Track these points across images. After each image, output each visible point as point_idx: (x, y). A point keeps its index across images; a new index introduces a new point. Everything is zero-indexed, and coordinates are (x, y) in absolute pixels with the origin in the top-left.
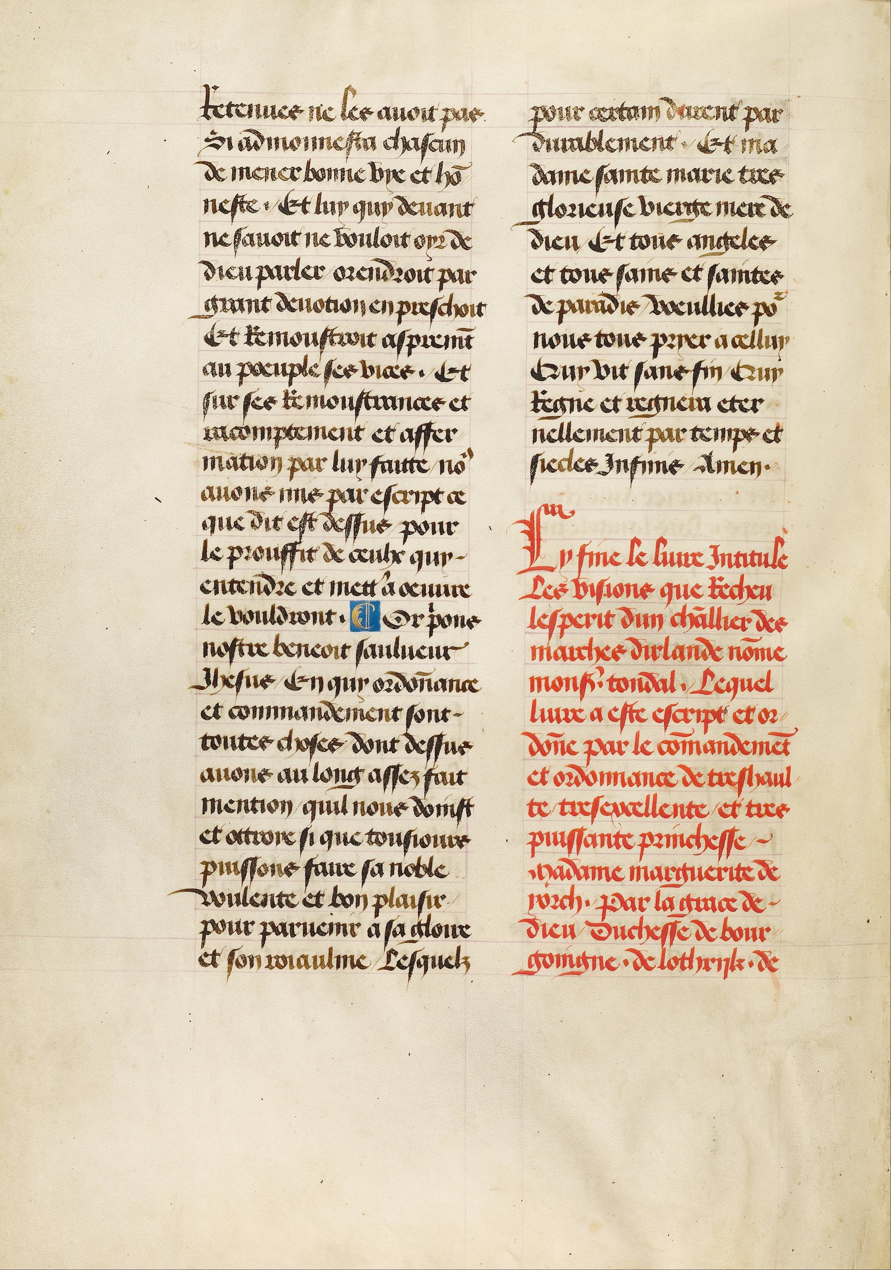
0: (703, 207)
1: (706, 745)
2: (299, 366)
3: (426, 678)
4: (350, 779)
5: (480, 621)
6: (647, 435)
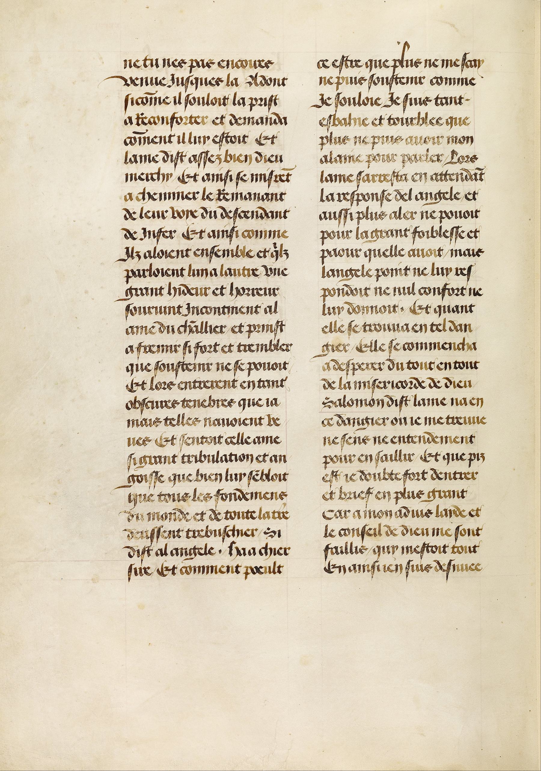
0: (444, 195)
2: (401, 493)
3: (434, 201)
5: (273, 63)
6: (247, 328)
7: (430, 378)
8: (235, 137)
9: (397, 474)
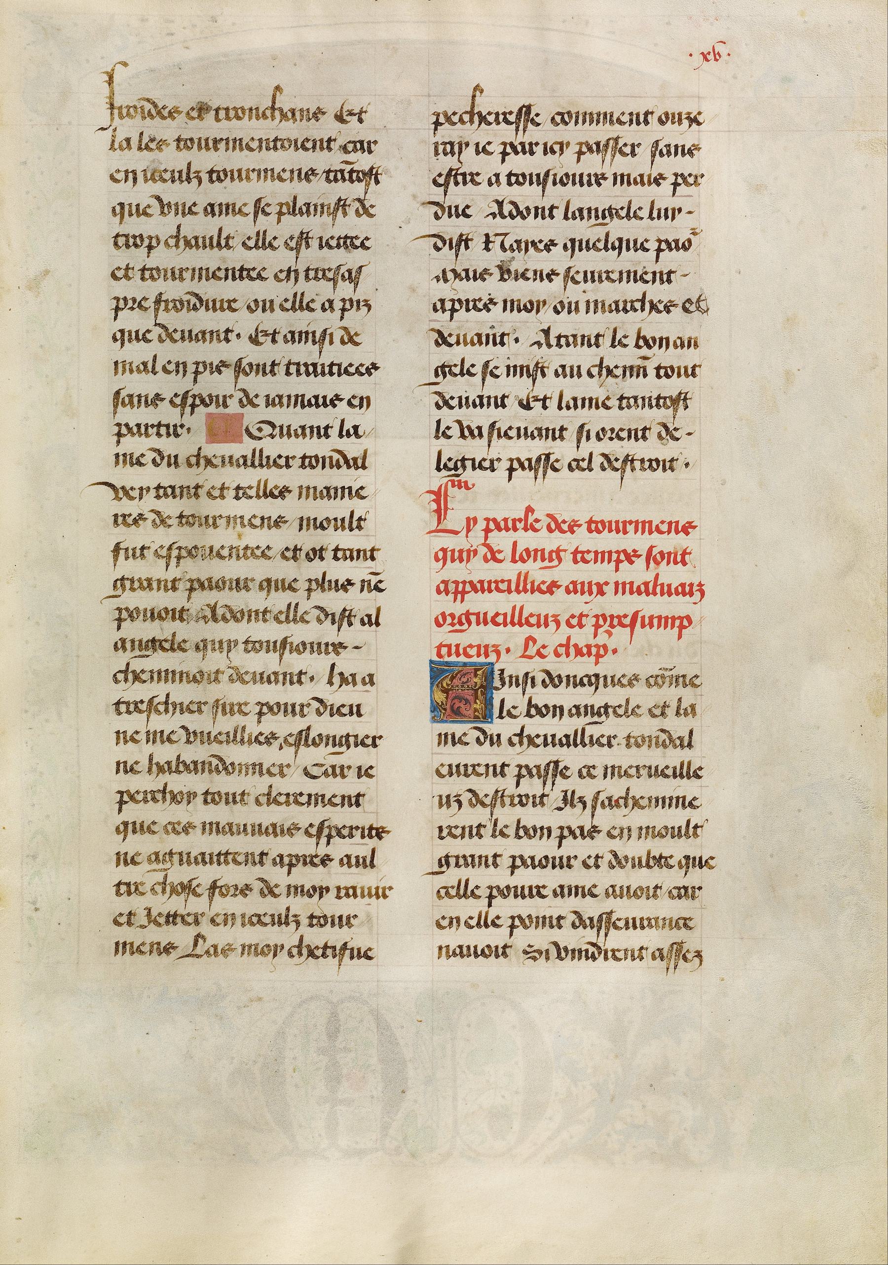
1: (574, 211)
3: (546, 563)
4: (341, 745)
7: (575, 912)
8: (219, 793)
9: (236, 853)
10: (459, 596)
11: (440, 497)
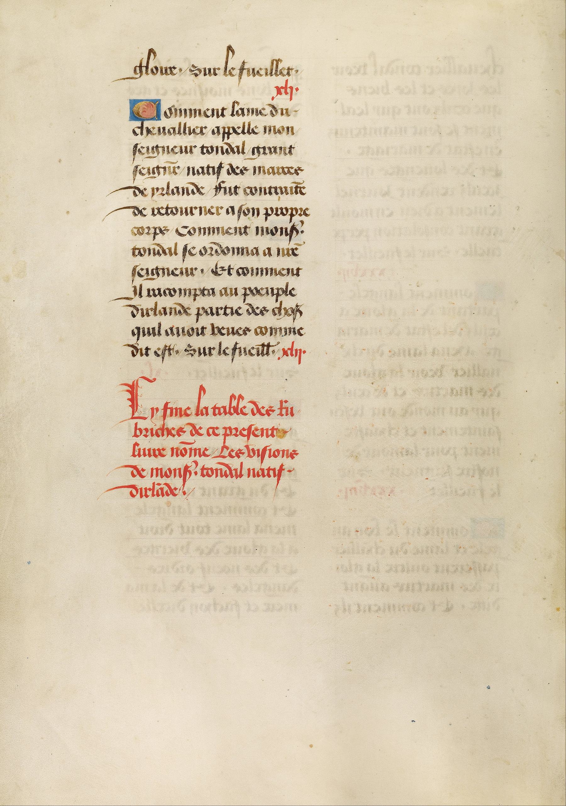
10: (226, 135)
11: (132, 389)
